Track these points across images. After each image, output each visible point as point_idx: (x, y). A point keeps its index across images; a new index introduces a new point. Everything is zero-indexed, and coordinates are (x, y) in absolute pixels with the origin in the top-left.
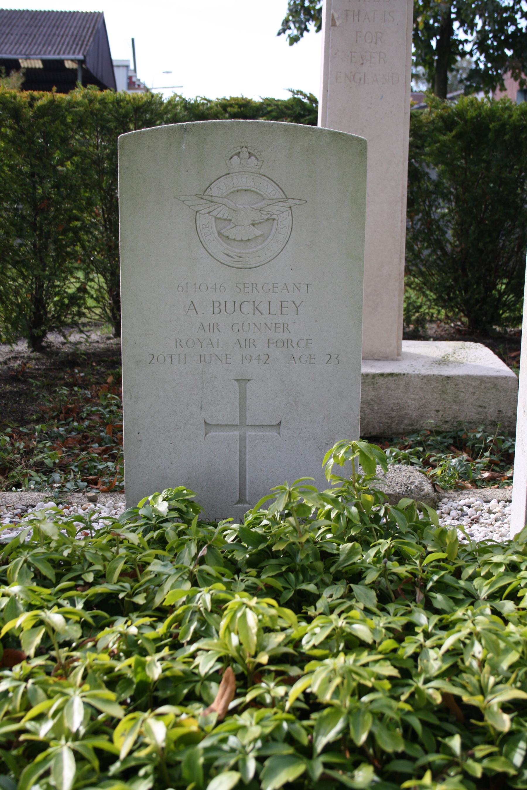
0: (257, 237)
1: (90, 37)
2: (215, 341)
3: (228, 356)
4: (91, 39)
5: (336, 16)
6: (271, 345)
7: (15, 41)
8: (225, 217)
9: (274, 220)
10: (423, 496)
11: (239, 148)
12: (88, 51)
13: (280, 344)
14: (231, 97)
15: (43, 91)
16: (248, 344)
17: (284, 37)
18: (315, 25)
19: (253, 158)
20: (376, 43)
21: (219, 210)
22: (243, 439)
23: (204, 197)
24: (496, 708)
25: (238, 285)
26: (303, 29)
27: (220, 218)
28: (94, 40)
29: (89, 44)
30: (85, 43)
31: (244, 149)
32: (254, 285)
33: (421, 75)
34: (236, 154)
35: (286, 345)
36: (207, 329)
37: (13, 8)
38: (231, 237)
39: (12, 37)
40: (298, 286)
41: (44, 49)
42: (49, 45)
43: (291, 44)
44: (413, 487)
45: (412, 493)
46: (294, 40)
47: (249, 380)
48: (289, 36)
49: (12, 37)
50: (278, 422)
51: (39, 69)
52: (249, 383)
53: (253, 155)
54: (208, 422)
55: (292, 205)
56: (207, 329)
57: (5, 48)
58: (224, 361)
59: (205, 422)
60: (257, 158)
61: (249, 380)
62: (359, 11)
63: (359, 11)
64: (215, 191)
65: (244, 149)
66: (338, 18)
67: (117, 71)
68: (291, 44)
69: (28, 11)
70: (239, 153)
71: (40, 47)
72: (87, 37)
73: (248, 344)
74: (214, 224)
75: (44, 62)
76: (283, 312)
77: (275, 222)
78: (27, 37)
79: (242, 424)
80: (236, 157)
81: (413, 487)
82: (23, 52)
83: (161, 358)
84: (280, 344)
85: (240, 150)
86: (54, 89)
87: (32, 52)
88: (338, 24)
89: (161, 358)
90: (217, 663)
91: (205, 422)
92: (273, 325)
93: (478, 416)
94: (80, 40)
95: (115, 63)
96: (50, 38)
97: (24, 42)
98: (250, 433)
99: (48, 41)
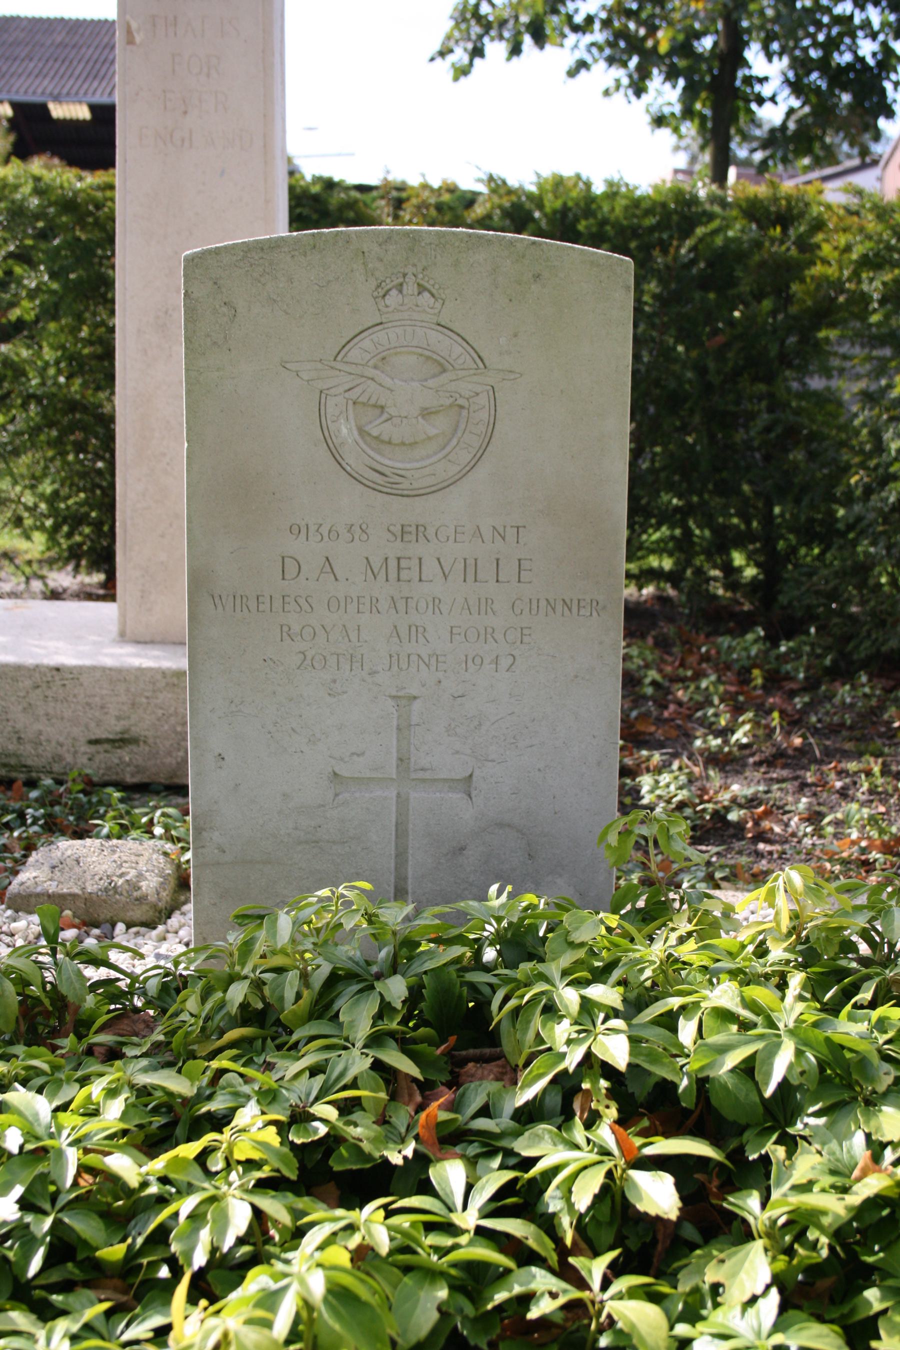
0: (429, 438)
5: (134, 25)
7: (36, 71)
8: (372, 401)
9: (461, 407)
10: (137, 899)
14: (610, 184)
17: (444, 66)
19: (426, 295)
20: (208, 75)
22: (402, 801)
23: (339, 365)
26: (478, 52)
27: (364, 404)
32: (421, 529)
35: (482, 637)
37: (44, 15)
38: (396, 439)
39: (32, 65)
40: (501, 530)
41: (86, 86)
42: (95, 77)
43: (456, 79)
44: (120, 882)
45: (116, 892)
46: (462, 72)
48: (453, 65)
49: (32, 65)
51: (84, 121)
53: (426, 289)
57: (18, 85)
60: (433, 295)
62: (175, 18)
63: (175, 18)
66: (139, 30)
68: (456, 79)
69: (62, 20)
71: (79, 82)
74: (351, 412)
75: (93, 108)
76: (479, 577)
77: (465, 413)
78: (57, 65)
81: (120, 882)
87: (65, 91)
88: (138, 39)
96: (98, 66)
97: (52, 73)
99: (94, 72)
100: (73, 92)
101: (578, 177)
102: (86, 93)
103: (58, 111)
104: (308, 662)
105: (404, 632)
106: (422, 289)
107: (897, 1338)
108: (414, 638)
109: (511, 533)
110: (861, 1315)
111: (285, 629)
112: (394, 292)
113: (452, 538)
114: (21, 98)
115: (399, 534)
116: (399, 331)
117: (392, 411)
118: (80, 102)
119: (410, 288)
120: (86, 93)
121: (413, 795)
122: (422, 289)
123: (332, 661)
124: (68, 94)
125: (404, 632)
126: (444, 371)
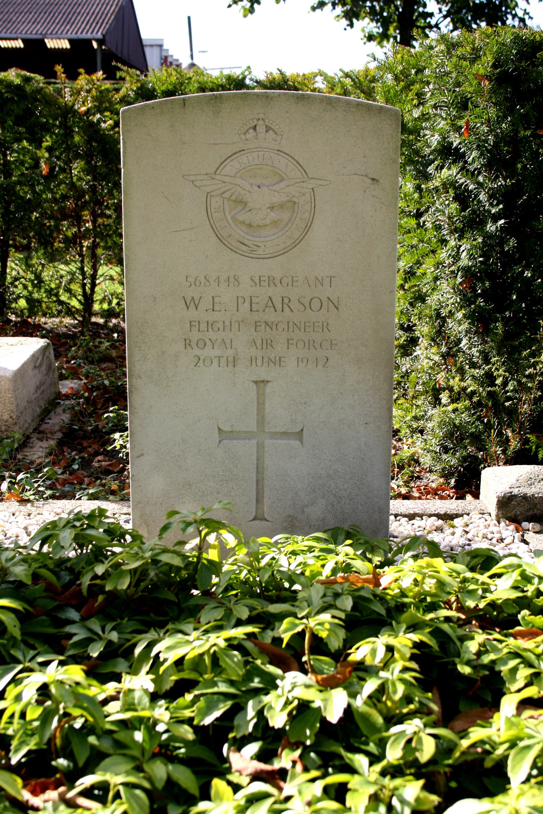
1: (112, 14)
2: (228, 341)
4: (113, 17)
11: (255, 120)
12: (108, 30)
18: (516, 581)
19: (271, 132)
25: (253, 278)
28: (115, 18)
29: (110, 22)
30: (106, 21)
31: (261, 122)
33: (28, 581)
35: (307, 345)
40: (320, 279)
53: (270, 128)
55: (314, 186)
59: (219, 429)
65: (261, 122)
67: (147, 51)
70: (256, 126)
72: (109, 15)
75: (71, 41)
82: (39, 32)
85: (255, 123)
87: (49, 32)
91: (219, 429)
92: (277, 359)
94: (100, 18)
95: (144, 43)
98: (269, 443)
100: (54, 32)
101: (177, 60)
102: (67, 33)
103: (51, 44)
104: (201, 361)
105: (259, 342)
106: (268, 129)
107: (234, 812)
108: (265, 347)
109: (327, 281)
110: (29, 787)
111: (188, 342)
112: (251, 131)
113: (290, 284)
114: (74, 36)
115: (257, 281)
116: (255, 155)
117: (250, 205)
118: (64, 39)
119: (261, 128)
120: (67, 33)
121: (267, 442)
122: (268, 129)
123: (215, 361)
124: (51, 33)
125: (259, 342)
126: (282, 180)
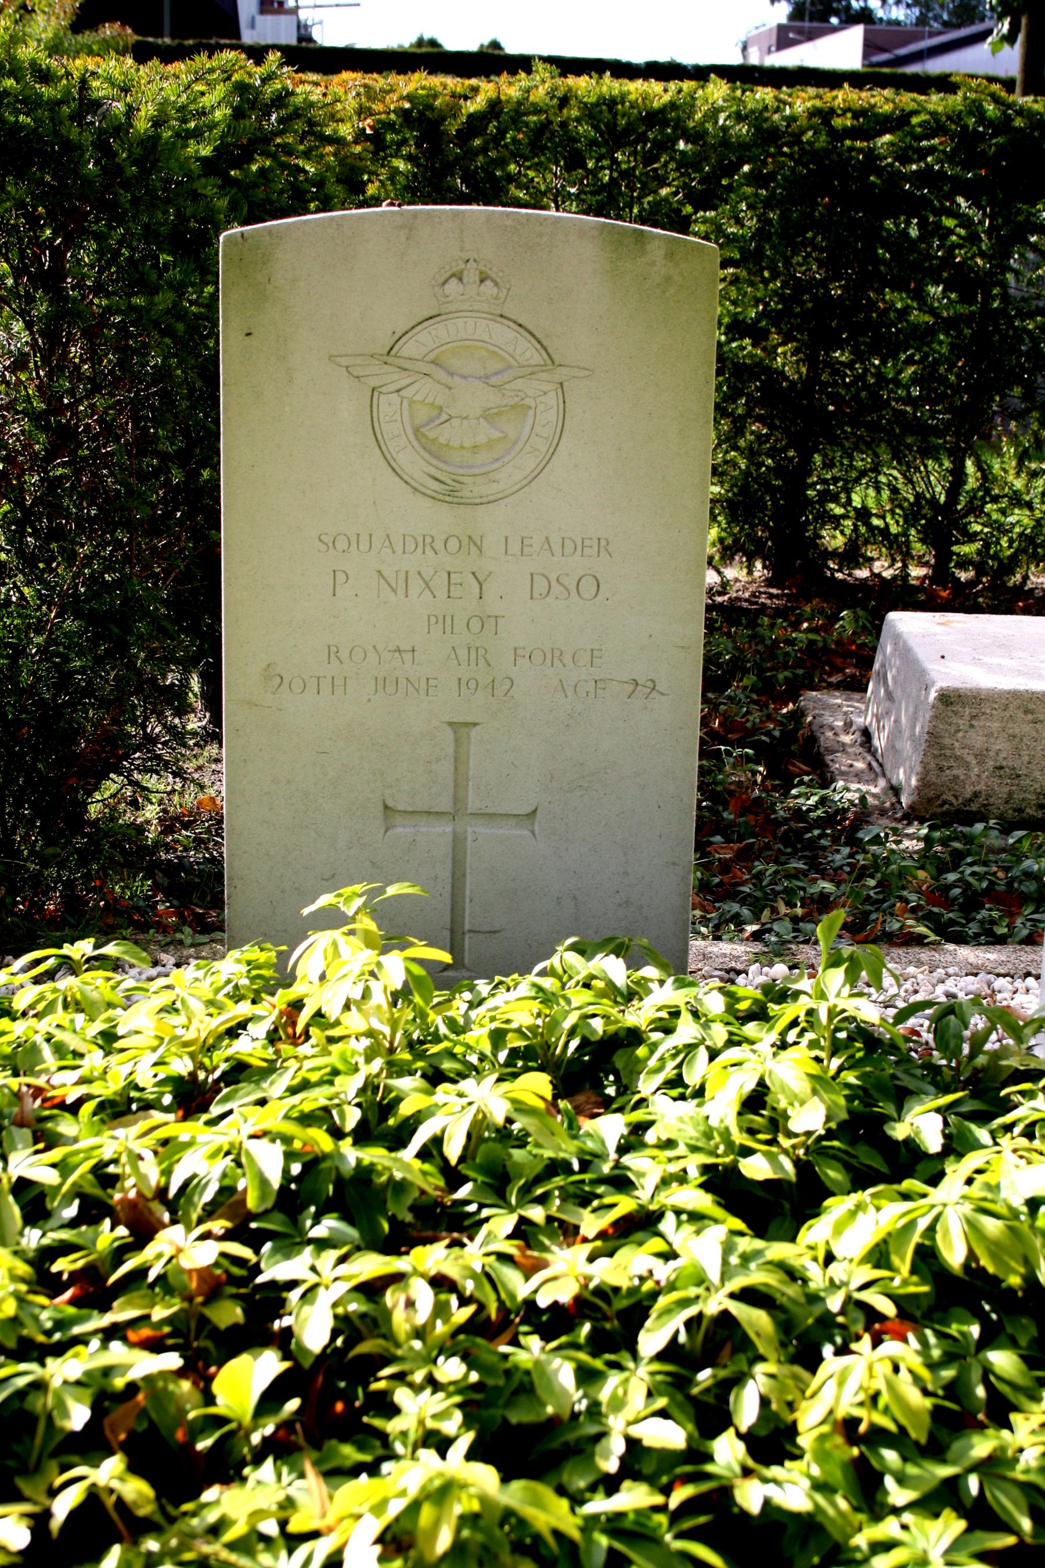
3: (432, 682)
6: (519, 661)
13: (538, 658)
15: (818, 86)
16: (473, 656)
19: (488, 283)
21: (417, 386)
22: (458, 842)
24: (808, 1457)
34: (452, 276)
36: (557, 548)
47: (475, 725)
50: (529, 810)
52: (474, 732)
54: (390, 803)
56: (557, 548)
58: (422, 692)
60: (496, 284)
61: (475, 725)
64: (409, 348)
73: (473, 656)
79: (457, 811)
80: (454, 281)
83: (297, 685)
84: (538, 658)
86: (846, 85)
89: (297, 685)
90: (355, 1295)
93: (211, 1517)
